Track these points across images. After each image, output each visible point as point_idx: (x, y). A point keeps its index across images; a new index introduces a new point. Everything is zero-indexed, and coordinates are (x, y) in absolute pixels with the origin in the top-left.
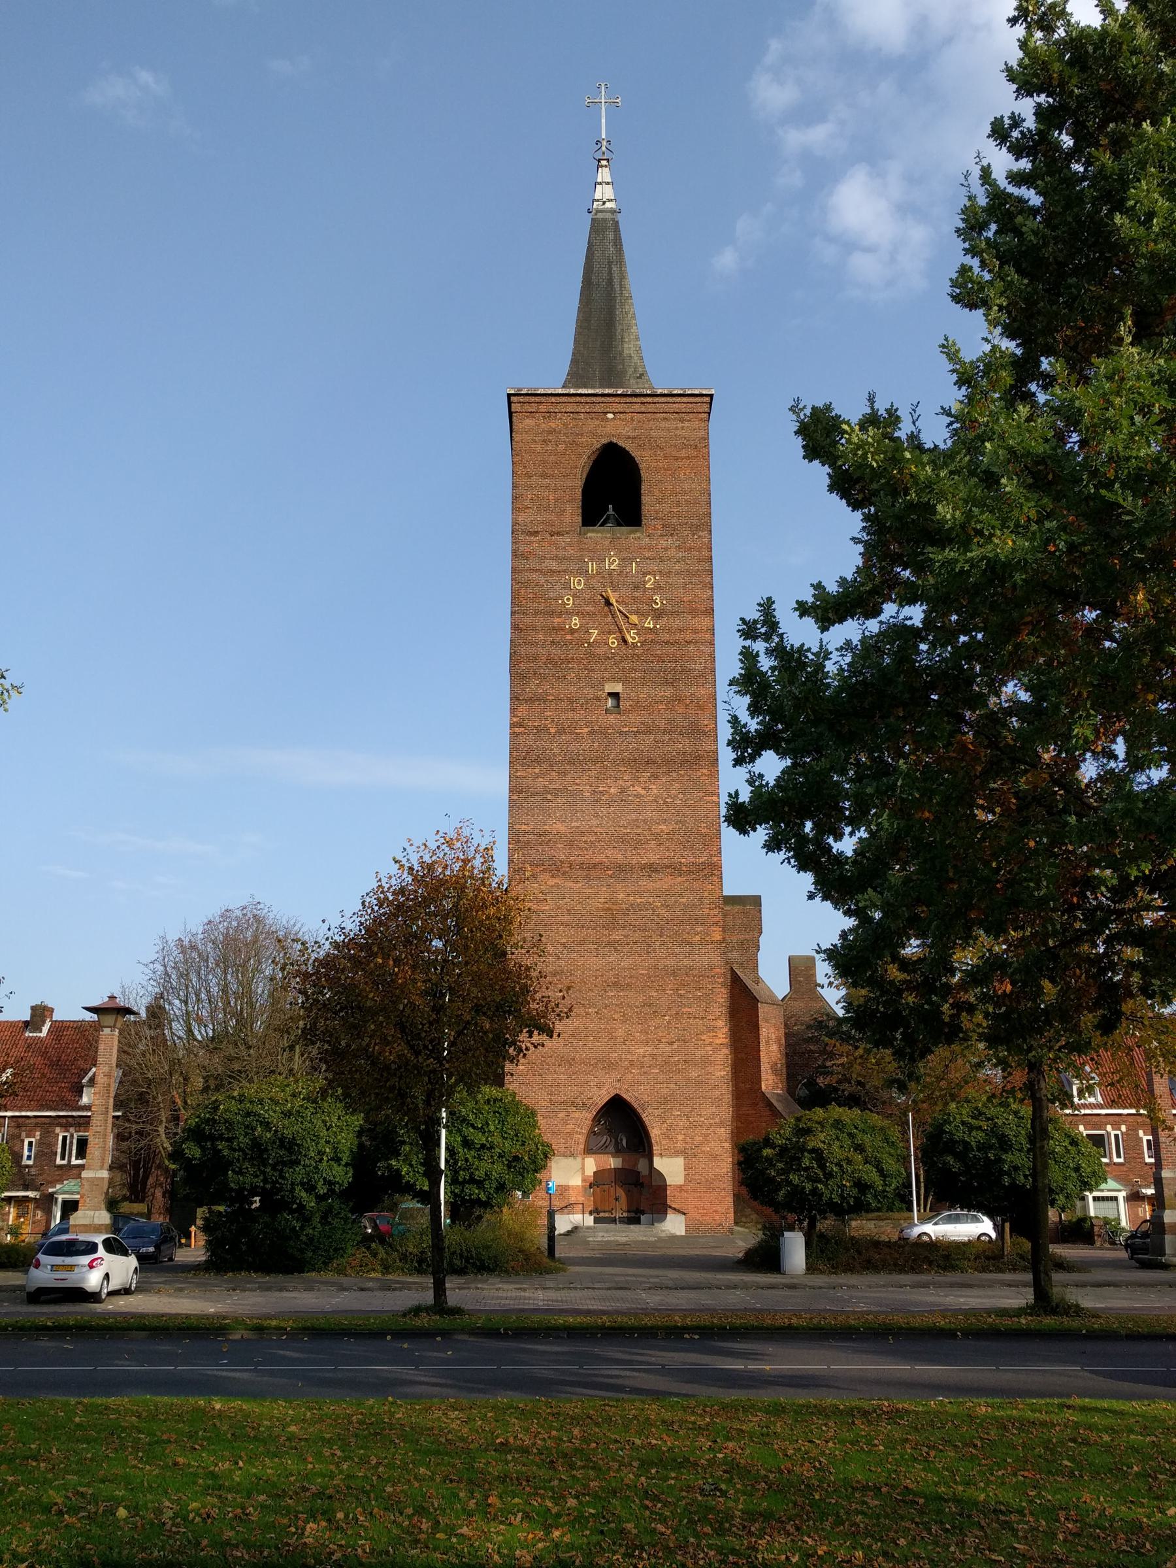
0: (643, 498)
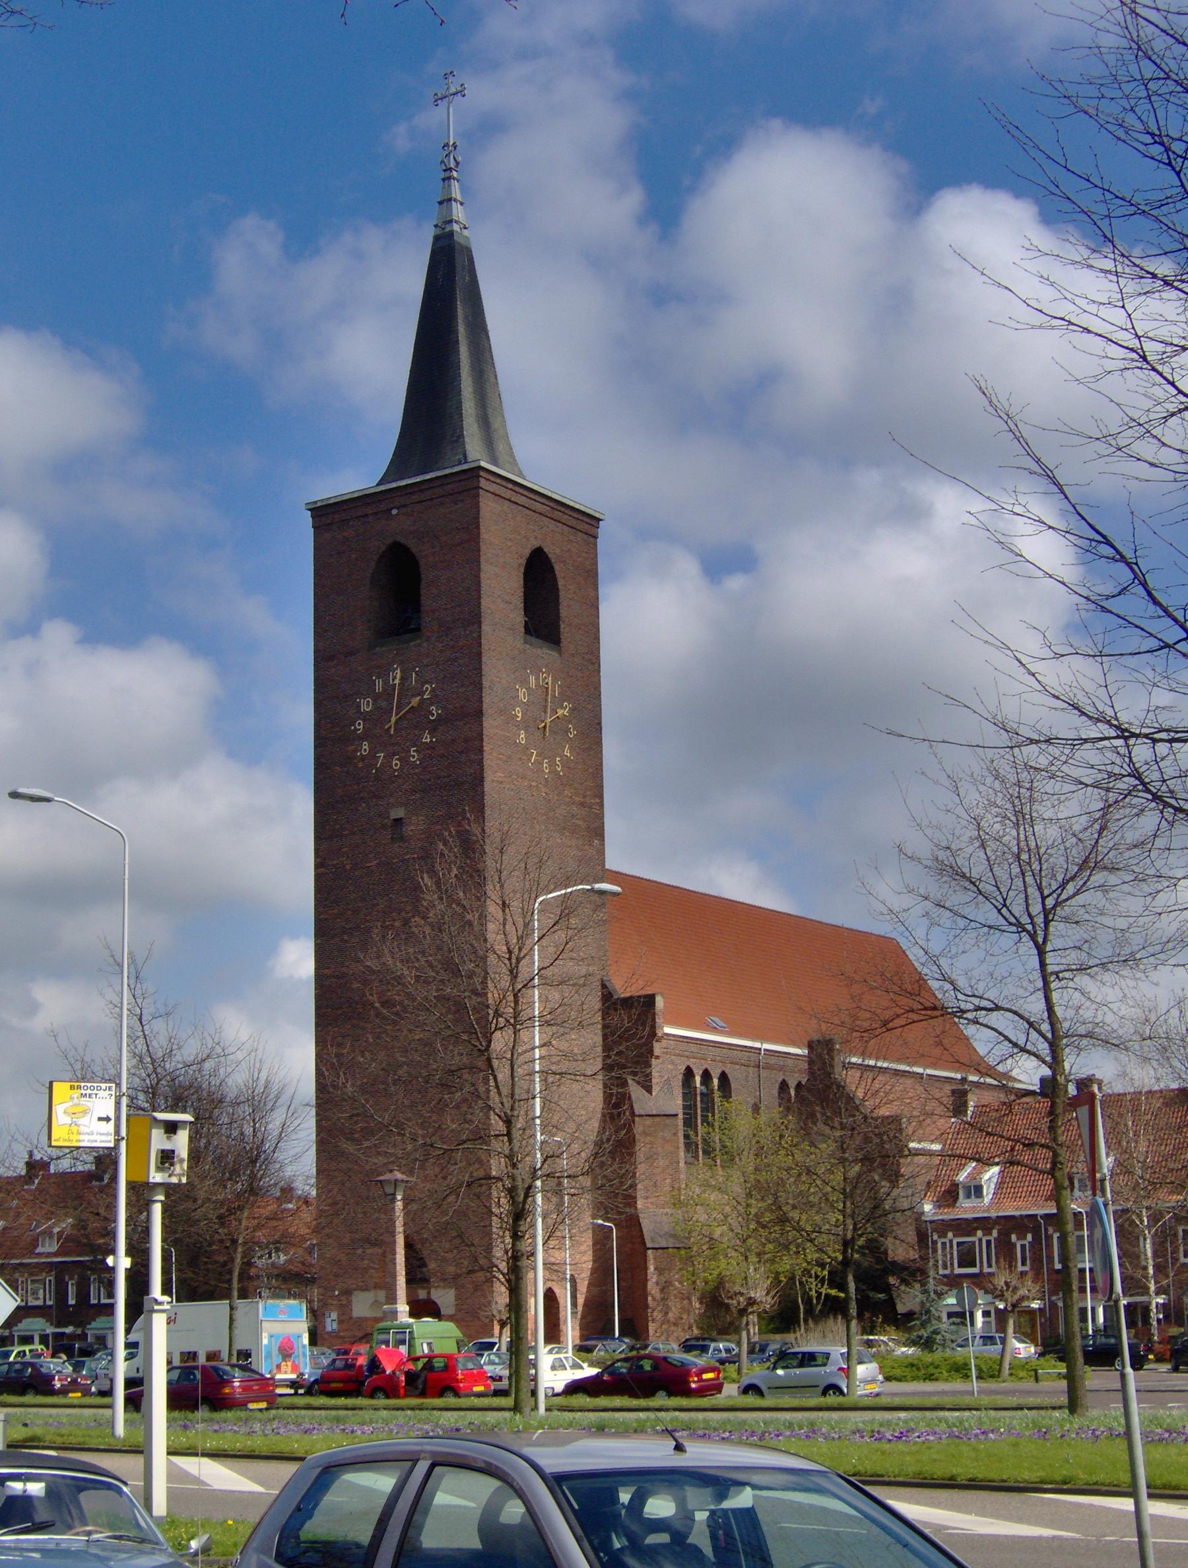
0: (422, 598)
